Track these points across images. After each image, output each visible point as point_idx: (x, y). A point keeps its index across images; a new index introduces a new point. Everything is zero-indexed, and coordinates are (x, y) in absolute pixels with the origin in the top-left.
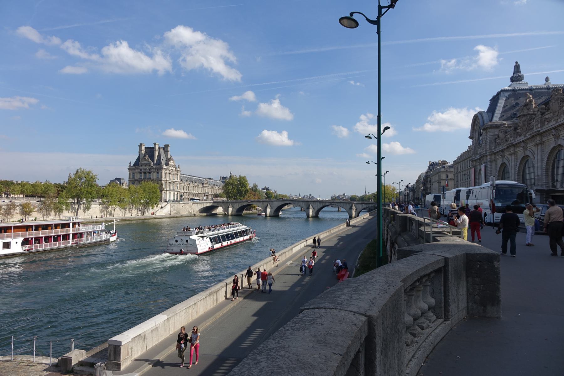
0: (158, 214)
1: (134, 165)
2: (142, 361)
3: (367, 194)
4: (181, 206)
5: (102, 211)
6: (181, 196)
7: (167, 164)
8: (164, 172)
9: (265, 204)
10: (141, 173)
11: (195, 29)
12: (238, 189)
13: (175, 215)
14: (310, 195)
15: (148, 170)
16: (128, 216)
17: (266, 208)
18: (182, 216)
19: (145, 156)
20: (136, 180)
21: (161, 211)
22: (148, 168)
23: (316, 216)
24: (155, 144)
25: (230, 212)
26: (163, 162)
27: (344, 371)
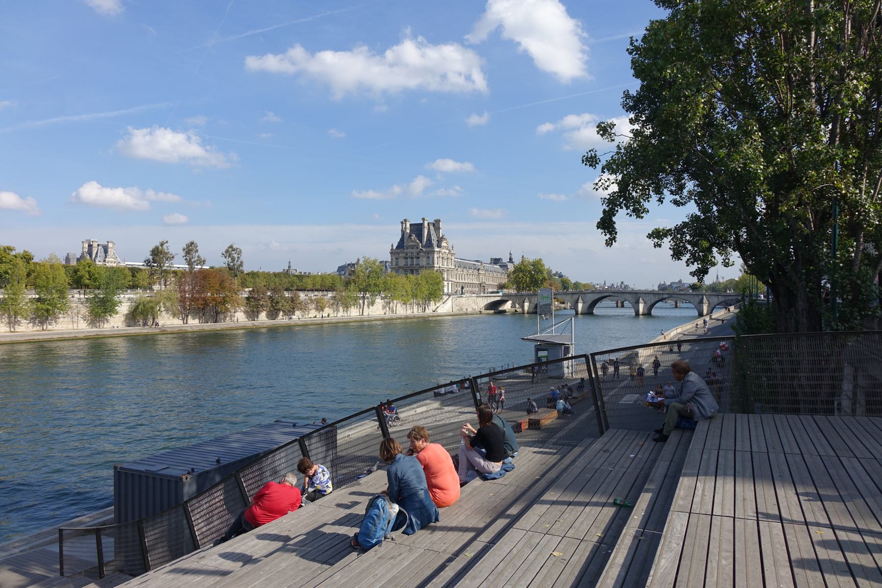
0: (441, 311)
1: (397, 248)
2: (277, 553)
3: (721, 281)
4: (463, 300)
5: (384, 308)
6: (462, 288)
7: (439, 246)
8: (436, 256)
9: (576, 297)
10: (406, 258)
11: (578, 114)
12: (532, 276)
13: (458, 312)
14: (622, 283)
15: (415, 254)
16: (409, 312)
17: (577, 302)
18: (466, 314)
19: (410, 236)
20: (400, 267)
21: (444, 307)
22: (416, 249)
23: (648, 314)
24: (423, 219)
25: (526, 308)
26: (435, 243)
27: (619, 585)
